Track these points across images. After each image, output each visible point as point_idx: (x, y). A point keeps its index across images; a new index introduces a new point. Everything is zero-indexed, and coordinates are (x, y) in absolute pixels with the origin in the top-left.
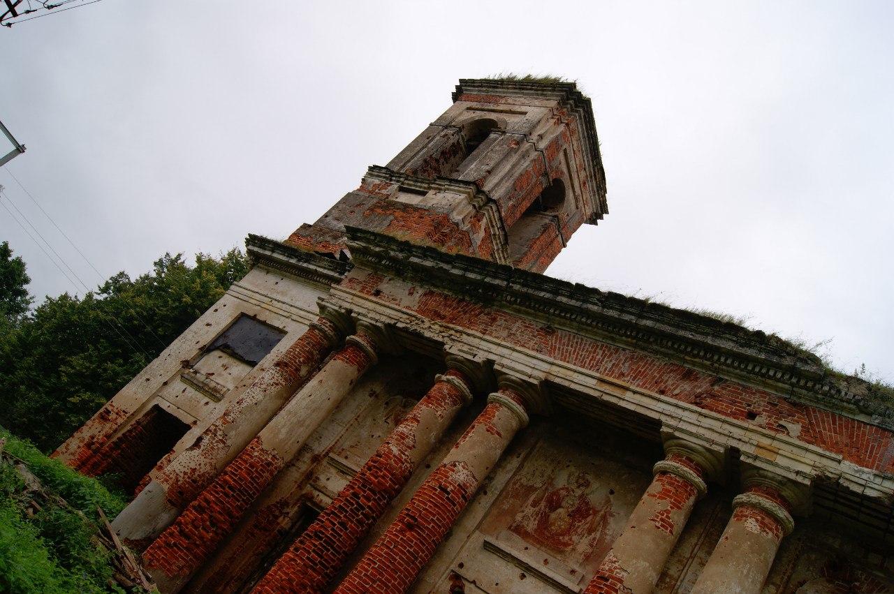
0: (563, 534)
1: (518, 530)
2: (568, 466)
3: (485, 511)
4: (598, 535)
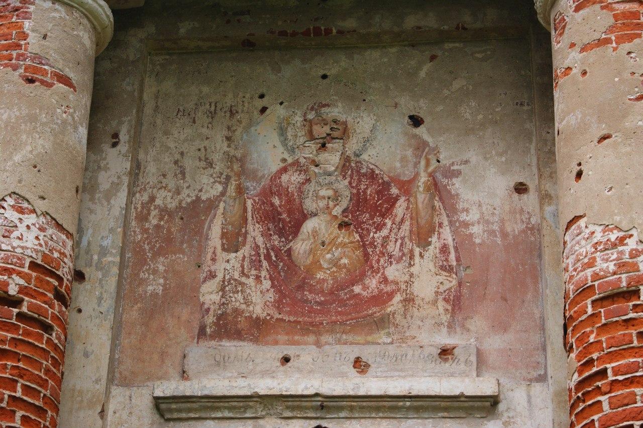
0: (359, 278)
1: (228, 326)
2: (264, 110)
3: (108, 324)
4: (447, 235)
